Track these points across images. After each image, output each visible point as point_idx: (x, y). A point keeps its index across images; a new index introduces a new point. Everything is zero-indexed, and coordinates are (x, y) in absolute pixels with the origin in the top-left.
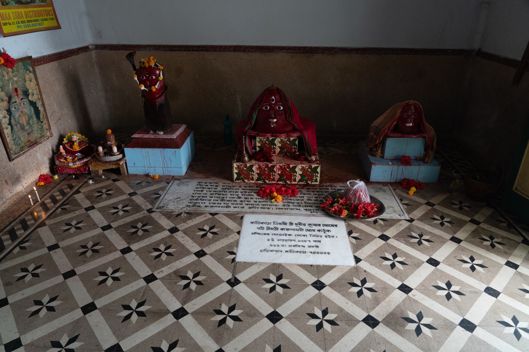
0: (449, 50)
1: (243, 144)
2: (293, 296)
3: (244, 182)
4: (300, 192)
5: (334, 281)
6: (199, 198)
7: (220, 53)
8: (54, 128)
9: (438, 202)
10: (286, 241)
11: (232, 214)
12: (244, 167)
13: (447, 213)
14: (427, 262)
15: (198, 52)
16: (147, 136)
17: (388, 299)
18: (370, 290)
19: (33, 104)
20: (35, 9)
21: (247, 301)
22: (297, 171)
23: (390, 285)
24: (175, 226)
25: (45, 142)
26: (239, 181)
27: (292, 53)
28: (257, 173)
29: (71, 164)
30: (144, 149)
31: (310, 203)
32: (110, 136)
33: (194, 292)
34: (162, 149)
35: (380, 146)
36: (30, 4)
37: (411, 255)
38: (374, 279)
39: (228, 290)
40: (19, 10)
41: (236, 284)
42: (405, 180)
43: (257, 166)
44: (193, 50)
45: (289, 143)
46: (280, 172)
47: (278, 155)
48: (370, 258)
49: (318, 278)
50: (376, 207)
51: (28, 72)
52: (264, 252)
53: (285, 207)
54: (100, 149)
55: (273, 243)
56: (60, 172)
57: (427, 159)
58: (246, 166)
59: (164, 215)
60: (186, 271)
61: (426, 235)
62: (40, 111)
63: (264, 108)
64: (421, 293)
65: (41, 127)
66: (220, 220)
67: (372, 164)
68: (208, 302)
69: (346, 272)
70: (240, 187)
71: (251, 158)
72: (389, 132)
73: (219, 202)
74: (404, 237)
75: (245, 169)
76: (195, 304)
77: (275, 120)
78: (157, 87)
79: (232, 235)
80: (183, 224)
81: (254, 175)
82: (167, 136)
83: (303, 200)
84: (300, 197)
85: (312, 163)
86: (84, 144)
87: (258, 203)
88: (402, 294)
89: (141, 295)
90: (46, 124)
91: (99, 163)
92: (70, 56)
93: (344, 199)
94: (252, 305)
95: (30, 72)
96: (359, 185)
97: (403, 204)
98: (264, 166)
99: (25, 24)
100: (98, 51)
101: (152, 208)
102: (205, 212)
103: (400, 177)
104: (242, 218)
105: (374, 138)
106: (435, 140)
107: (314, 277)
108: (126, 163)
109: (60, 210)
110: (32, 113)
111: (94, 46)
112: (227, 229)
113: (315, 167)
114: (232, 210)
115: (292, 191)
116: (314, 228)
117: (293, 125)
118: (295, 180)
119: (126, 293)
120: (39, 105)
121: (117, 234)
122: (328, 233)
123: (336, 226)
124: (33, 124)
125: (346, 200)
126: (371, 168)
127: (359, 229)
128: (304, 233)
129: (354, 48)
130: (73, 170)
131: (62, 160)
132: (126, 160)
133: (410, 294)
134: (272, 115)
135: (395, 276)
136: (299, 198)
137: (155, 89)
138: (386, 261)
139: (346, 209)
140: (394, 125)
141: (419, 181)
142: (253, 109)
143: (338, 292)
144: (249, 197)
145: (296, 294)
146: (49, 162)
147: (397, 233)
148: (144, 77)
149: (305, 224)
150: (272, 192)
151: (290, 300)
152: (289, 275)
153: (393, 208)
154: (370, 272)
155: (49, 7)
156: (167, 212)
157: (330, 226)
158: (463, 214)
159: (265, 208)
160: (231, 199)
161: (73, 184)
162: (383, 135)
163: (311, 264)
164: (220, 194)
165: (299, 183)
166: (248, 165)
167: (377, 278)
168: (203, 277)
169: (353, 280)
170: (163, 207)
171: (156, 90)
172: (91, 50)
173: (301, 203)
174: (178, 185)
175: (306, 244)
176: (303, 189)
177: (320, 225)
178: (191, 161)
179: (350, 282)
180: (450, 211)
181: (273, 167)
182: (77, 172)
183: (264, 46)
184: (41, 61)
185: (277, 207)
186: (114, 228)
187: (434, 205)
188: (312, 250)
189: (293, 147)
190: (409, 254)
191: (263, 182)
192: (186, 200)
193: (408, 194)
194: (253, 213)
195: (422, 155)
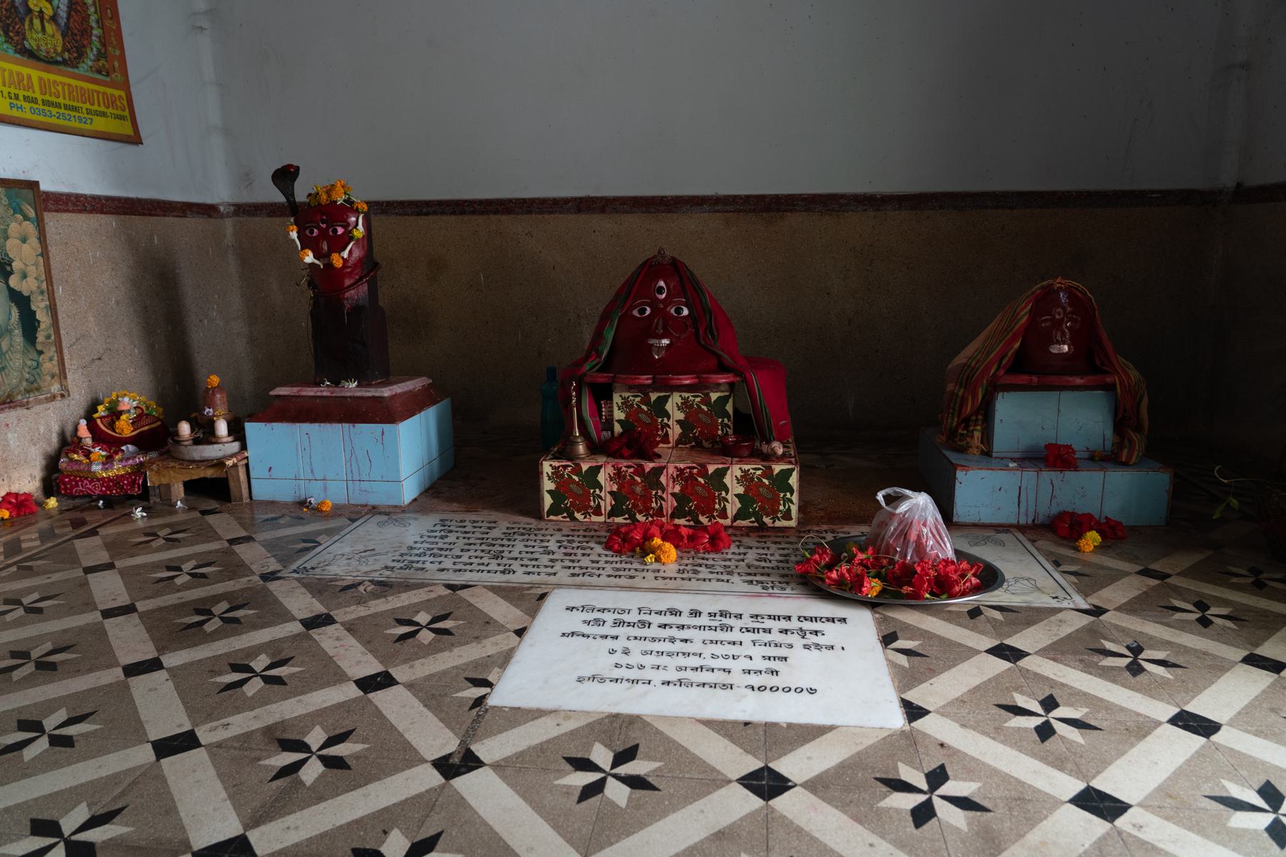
0: (1153, 192)
1: (572, 407)
2: (664, 814)
3: (574, 519)
4: (737, 543)
5: (827, 772)
6: (429, 552)
7: (540, 217)
8: (77, 376)
9: (1178, 570)
10: (670, 654)
11: (514, 588)
12: (573, 472)
13: (1215, 594)
14: (1174, 721)
15: (485, 217)
16: (312, 391)
17: (1034, 837)
18: (963, 803)
19: (20, 301)
20: (74, 82)
21: (486, 824)
22: (729, 485)
23: (1040, 791)
24: (324, 611)
25: (38, 408)
26: (560, 518)
27: (727, 212)
28: (611, 493)
29: (96, 468)
30: (298, 425)
31: (763, 568)
32: (213, 392)
33: (308, 788)
34: (347, 425)
35: (976, 420)
36: (60, 67)
37: (1108, 702)
38: (973, 768)
39: (428, 787)
40: (25, 71)
41: (463, 770)
42: (1063, 516)
43: (610, 470)
44: (474, 212)
45: (706, 409)
46: (677, 489)
47: (677, 445)
48: (958, 709)
49: (767, 759)
50: (974, 575)
51: (20, 217)
52: (587, 684)
53: (685, 575)
54: (185, 428)
55: (624, 660)
56: (66, 489)
57: (1125, 452)
58: (577, 470)
59: (305, 587)
60: (307, 726)
61: (1152, 647)
62: (39, 322)
63: (635, 313)
64: (1167, 819)
65: (35, 364)
66: (472, 601)
67: (954, 467)
68: (343, 822)
69: (871, 746)
70: (559, 530)
71: (595, 448)
72: (1002, 372)
73: (485, 561)
74: (1075, 653)
75: (576, 478)
76: (292, 827)
77: (665, 342)
78: (345, 254)
79: (497, 637)
80: (353, 608)
81: (601, 498)
82: (366, 391)
83: (743, 560)
84: (734, 553)
85: (773, 461)
86: (148, 421)
87: (601, 564)
88: (1091, 821)
89: (117, 791)
90: (51, 359)
91: (172, 464)
92: (158, 215)
93: (870, 550)
94: (501, 839)
95: (26, 218)
96: (913, 501)
97: (1064, 572)
98: (631, 470)
99: (35, 106)
100: (241, 219)
101: (279, 571)
102: (434, 582)
103: (1046, 509)
104: (542, 597)
105: (957, 395)
106: (1145, 401)
107: (750, 757)
108: (247, 465)
109: (14, 569)
110: (12, 321)
111: (232, 208)
112: (488, 623)
113: (782, 470)
114: (519, 577)
115: (710, 538)
116: (768, 624)
117: (718, 356)
118: (723, 514)
119: (74, 783)
120: (39, 307)
121: (142, 627)
122: (812, 639)
123: (843, 620)
124: (9, 349)
125: (877, 551)
126: (955, 478)
127: (919, 629)
128: (735, 635)
129: (891, 196)
130: (102, 485)
131: (76, 456)
132: (247, 458)
133: (1121, 822)
134: (656, 328)
135: (1059, 763)
136: (730, 556)
137: (341, 261)
138: (1018, 717)
139: (878, 576)
140: (1013, 350)
141: (1106, 518)
142: (605, 318)
143: (836, 807)
144: (580, 552)
145: (675, 809)
146: (44, 463)
147: (1051, 641)
148: (316, 231)
149: (741, 615)
150: (648, 537)
151: (649, 829)
152: (661, 749)
153: (1033, 582)
154: (962, 749)
155: (117, 88)
156: (320, 579)
157: (823, 620)
158: (1269, 598)
159: (620, 577)
160: (524, 555)
161: (87, 519)
162: (985, 382)
163: (747, 718)
164: (494, 545)
165: (735, 524)
166: (585, 467)
167: (989, 766)
168: (356, 745)
169: (898, 772)
170: (313, 568)
171: (345, 266)
172: (222, 216)
173: (737, 567)
174: (380, 524)
175: (736, 666)
176: (748, 536)
177: (789, 618)
178: (436, 476)
179: (884, 776)
180: (1227, 590)
181: (658, 471)
182: (111, 491)
183: (653, 198)
184: (67, 204)
185: (657, 574)
186: (139, 614)
187: (1169, 576)
188: (755, 680)
189: (720, 420)
190: (1102, 700)
191: (628, 521)
192: (390, 555)
193: (1077, 549)
194: (580, 586)
195: (1109, 445)
